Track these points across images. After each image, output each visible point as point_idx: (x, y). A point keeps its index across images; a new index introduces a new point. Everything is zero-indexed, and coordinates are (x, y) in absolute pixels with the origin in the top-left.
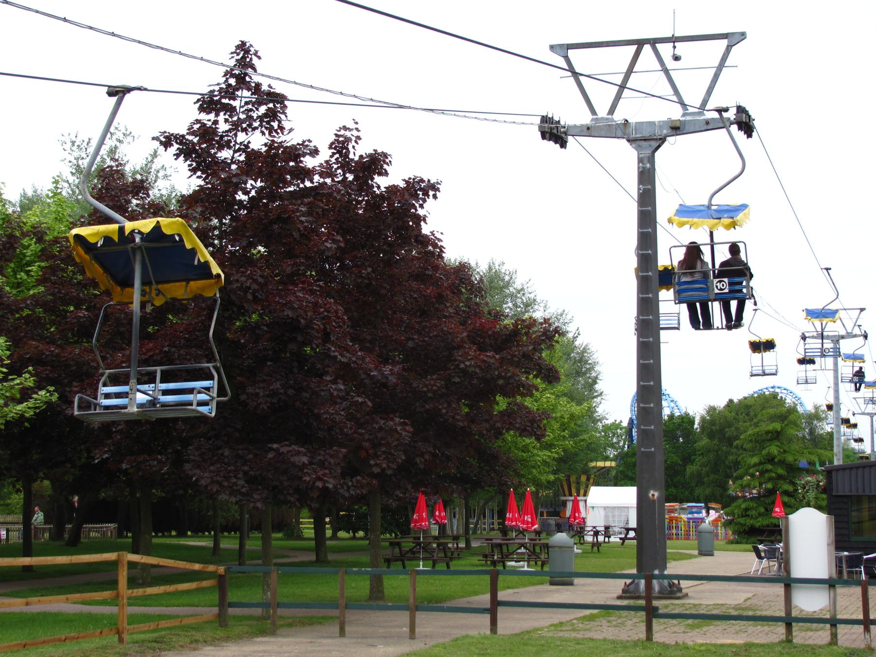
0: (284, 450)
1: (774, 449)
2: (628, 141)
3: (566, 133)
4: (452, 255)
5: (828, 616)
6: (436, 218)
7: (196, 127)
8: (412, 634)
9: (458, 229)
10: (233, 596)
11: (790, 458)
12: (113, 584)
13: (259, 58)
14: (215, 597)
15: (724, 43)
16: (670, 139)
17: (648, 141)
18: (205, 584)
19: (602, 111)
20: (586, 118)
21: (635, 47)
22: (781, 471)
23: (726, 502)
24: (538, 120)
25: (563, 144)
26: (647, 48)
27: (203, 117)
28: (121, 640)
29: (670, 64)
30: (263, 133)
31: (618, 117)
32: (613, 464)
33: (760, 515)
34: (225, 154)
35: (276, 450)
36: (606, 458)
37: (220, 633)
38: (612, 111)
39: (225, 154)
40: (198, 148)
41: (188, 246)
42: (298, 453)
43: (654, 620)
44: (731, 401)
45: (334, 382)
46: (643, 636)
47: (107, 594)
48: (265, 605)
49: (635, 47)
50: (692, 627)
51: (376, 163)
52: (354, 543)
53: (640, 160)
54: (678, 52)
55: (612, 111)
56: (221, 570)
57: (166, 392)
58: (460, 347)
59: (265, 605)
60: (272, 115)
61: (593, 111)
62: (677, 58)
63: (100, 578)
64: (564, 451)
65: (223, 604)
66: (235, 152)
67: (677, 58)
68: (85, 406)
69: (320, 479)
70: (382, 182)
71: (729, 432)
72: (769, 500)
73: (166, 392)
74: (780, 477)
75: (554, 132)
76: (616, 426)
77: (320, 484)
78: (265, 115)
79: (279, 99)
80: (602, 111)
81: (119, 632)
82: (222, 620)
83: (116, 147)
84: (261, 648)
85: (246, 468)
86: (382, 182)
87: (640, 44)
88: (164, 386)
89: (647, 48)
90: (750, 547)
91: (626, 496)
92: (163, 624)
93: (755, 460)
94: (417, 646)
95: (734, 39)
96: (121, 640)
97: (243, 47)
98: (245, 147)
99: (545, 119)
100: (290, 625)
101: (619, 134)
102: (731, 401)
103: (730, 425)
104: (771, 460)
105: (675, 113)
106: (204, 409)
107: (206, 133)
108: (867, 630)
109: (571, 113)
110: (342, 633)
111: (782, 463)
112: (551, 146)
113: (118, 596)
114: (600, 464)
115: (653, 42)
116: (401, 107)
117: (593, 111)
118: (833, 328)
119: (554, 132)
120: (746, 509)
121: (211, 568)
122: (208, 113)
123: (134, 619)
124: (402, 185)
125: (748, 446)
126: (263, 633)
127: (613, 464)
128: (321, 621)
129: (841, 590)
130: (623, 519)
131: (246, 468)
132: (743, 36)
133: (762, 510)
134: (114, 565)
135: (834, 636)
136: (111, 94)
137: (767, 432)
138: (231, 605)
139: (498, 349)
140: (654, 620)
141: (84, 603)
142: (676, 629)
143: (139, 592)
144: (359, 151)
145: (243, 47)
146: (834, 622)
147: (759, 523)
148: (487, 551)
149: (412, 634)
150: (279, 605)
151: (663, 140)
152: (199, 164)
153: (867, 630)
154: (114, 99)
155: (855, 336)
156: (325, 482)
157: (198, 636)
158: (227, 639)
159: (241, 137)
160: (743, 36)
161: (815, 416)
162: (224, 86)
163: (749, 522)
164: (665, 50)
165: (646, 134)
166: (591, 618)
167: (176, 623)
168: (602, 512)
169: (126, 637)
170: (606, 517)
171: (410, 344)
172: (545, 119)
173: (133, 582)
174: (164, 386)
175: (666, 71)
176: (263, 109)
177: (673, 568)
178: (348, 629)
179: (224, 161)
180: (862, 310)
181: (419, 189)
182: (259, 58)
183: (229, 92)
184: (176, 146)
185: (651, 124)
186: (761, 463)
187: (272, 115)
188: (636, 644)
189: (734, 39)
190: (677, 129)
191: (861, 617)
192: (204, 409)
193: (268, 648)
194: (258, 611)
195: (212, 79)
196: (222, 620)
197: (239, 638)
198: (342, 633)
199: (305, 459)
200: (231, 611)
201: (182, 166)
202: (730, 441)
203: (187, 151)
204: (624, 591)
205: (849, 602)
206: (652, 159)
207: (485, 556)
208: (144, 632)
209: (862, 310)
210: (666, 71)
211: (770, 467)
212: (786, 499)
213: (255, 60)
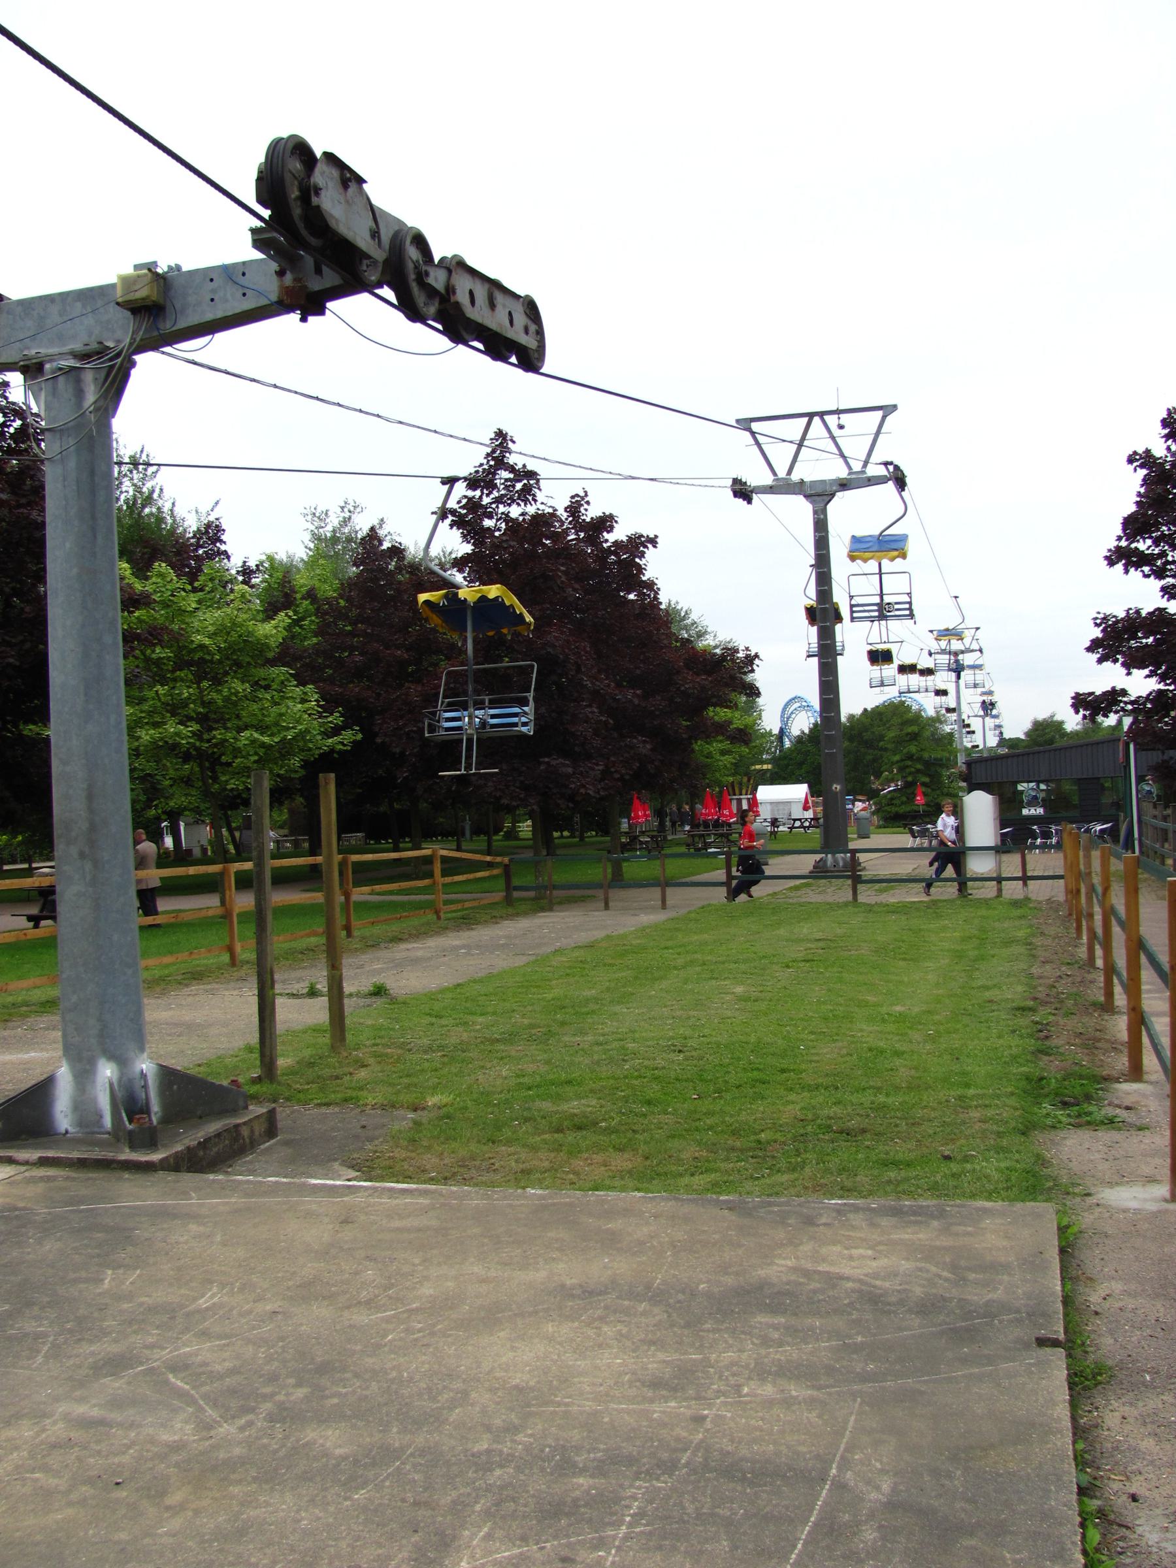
0: (554, 763)
1: (913, 749)
2: (805, 496)
3: (752, 492)
4: (666, 597)
5: (995, 875)
6: (653, 565)
7: (464, 501)
8: (664, 905)
9: (673, 579)
10: (516, 882)
11: (926, 755)
12: (430, 875)
13: (514, 442)
14: (502, 883)
15: (880, 413)
16: (839, 494)
17: (820, 495)
18: (496, 872)
19: (782, 473)
20: (768, 480)
21: (806, 419)
22: (919, 766)
23: (872, 795)
24: (730, 482)
25: (749, 501)
26: (816, 419)
27: (470, 493)
28: (439, 918)
29: (836, 432)
30: (519, 505)
31: (795, 477)
32: (770, 767)
33: (903, 803)
34: (488, 523)
35: (548, 763)
36: (762, 762)
37: (510, 910)
38: (790, 472)
39: (488, 523)
40: (468, 520)
41: (508, 603)
42: (568, 766)
43: (859, 886)
44: (865, 710)
45: (590, 706)
46: (850, 898)
47: (427, 882)
48: (536, 888)
49: (806, 419)
50: (881, 891)
51: (605, 522)
52: (564, 840)
53: (815, 512)
54: (841, 422)
55: (790, 472)
56: (506, 860)
57: (493, 717)
58: (678, 672)
59: (536, 888)
60: (527, 490)
61: (775, 474)
62: (841, 427)
63: (422, 868)
64: (741, 756)
65: (509, 888)
66: (498, 520)
67: (841, 427)
68: (432, 729)
69: (583, 786)
70: (611, 537)
71: (867, 736)
72: (909, 791)
73: (493, 717)
74: (918, 771)
75: (742, 491)
76: (770, 733)
77: (582, 791)
78: (522, 490)
79: (532, 475)
80: (782, 473)
81: (437, 912)
82: (509, 901)
83: (350, 518)
84: (542, 920)
85: (522, 778)
86: (611, 537)
87: (811, 416)
88: (492, 712)
89: (816, 419)
90: (905, 826)
91: (798, 792)
92: (467, 905)
93: (897, 758)
94: (671, 914)
95: (888, 410)
96: (439, 918)
97: (500, 434)
98: (507, 518)
99: (736, 481)
100: (560, 903)
101: (797, 490)
102: (865, 710)
103: (866, 730)
104: (910, 757)
105: (843, 473)
106: (524, 729)
107: (473, 505)
108: (1025, 884)
109: (757, 476)
110: (607, 907)
111: (920, 759)
112: (740, 502)
113: (434, 883)
114: (758, 767)
115: (821, 414)
116: (634, 478)
117: (775, 474)
118: (956, 645)
119: (742, 491)
120: (892, 799)
121: (499, 859)
122: (475, 490)
123: (446, 902)
124: (625, 539)
125: (890, 746)
126: (543, 909)
127: (770, 767)
128: (582, 899)
129: (1005, 858)
130: (786, 812)
131: (522, 778)
132: (894, 408)
133: (904, 799)
134: (428, 860)
135: (1000, 890)
136: (443, 483)
137: (908, 734)
138: (516, 888)
139: (709, 673)
140: (859, 886)
141: (400, 892)
142: (869, 893)
143: (448, 880)
144: (591, 512)
145: (500, 434)
146: (999, 880)
147: (903, 809)
148: (690, 840)
149: (664, 905)
150: (555, 887)
151: (833, 495)
152: (469, 532)
153: (1025, 884)
154: (447, 487)
155: (973, 651)
156: (587, 789)
157: (495, 913)
158: (517, 915)
159: (502, 509)
160: (894, 408)
161: (938, 719)
162: (486, 467)
163: (894, 809)
164: (832, 420)
165: (819, 490)
166: (797, 888)
167: (475, 904)
168: (769, 807)
169: (442, 915)
170: (772, 811)
171: (638, 672)
172: (736, 481)
173: (445, 873)
174: (492, 712)
175: (833, 438)
176: (519, 486)
177: (851, 846)
178: (611, 904)
179: (489, 528)
180: (977, 629)
181: (637, 544)
182: (514, 442)
183: (491, 472)
184: (450, 518)
185: (823, 482)
186: (902, 760)
187: (527, 490)
188: (846, 904)
189: (888, 410)
190: (844, 485)
191: (1020, 875)
192: (524, 729)
193: (548, 920)
194: (532, 894)
195: (472, 460)
196: (509, 901)
197: (525, 914)
198: (607, 907)
199: (570, 770)
200: (516, 894)
201: (456, 533)
202: (869, 744)
203: (459, 523)
204: (814, 867)
205: (1011, 864)
206: (824, 511)
207: (688, 845)
208: (454, 911)
209: (977, 629)
210: (833, 438)
211: (910, 763)
212: (923, 789)
213: (510, 445)
